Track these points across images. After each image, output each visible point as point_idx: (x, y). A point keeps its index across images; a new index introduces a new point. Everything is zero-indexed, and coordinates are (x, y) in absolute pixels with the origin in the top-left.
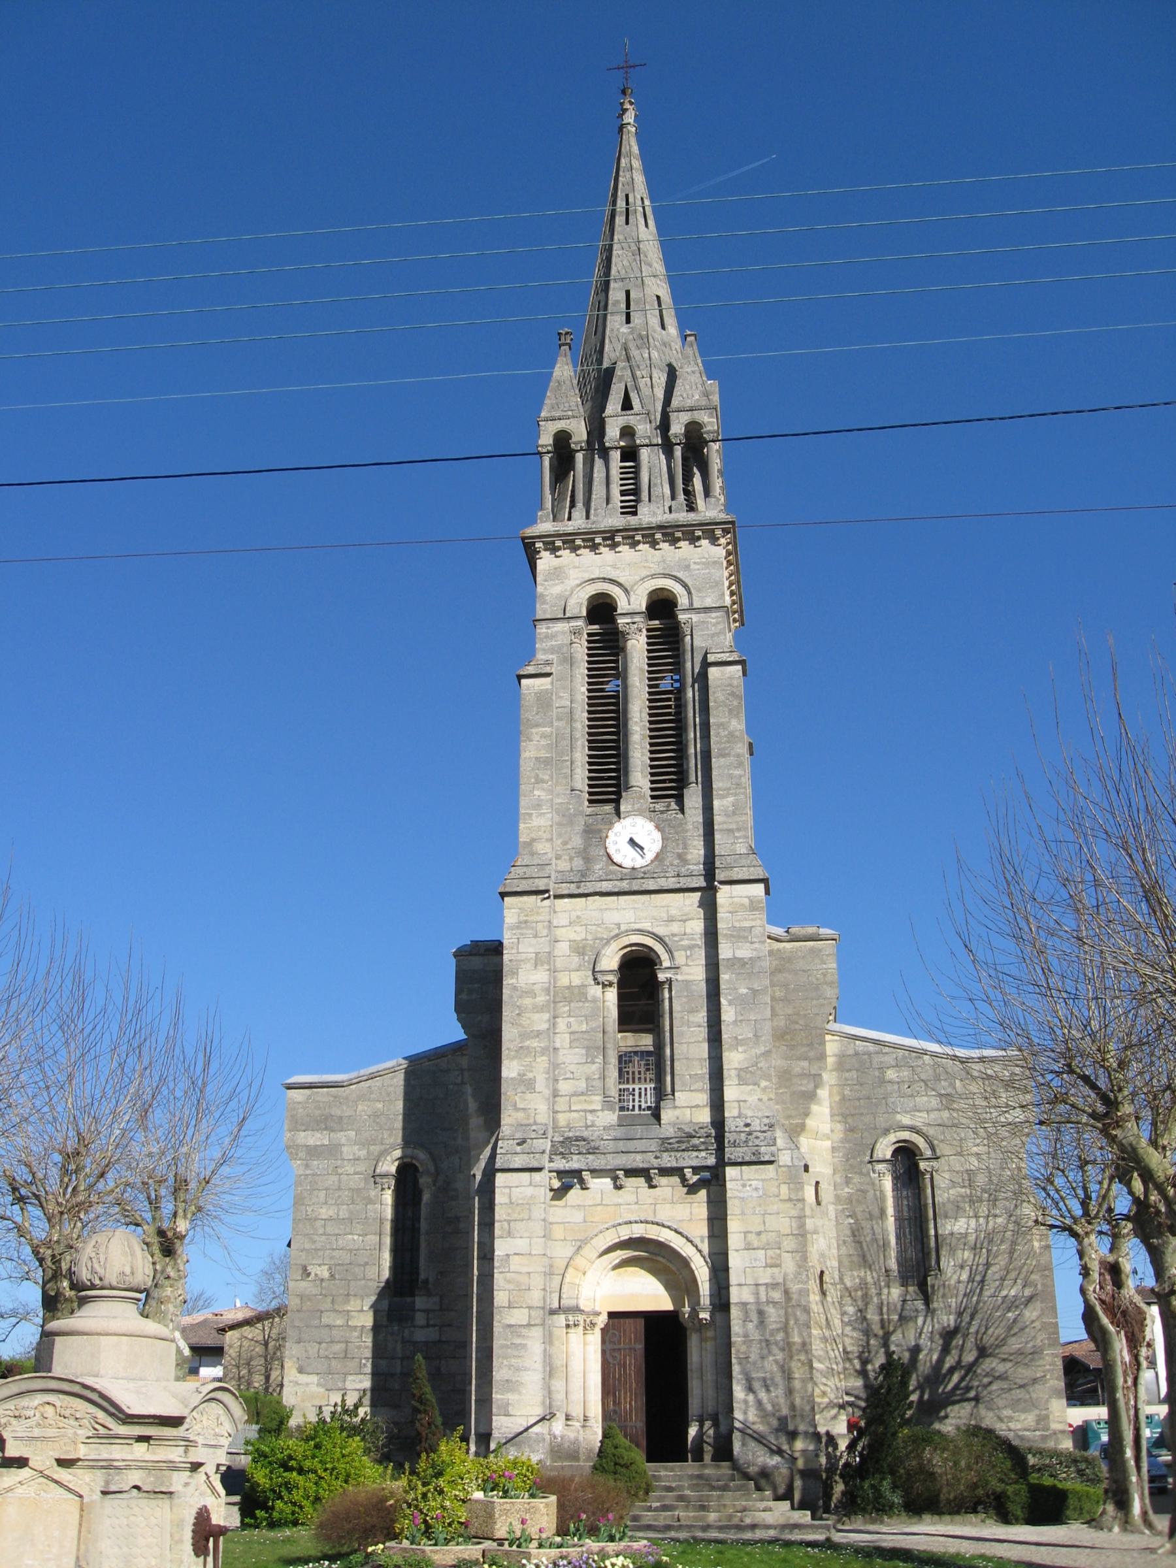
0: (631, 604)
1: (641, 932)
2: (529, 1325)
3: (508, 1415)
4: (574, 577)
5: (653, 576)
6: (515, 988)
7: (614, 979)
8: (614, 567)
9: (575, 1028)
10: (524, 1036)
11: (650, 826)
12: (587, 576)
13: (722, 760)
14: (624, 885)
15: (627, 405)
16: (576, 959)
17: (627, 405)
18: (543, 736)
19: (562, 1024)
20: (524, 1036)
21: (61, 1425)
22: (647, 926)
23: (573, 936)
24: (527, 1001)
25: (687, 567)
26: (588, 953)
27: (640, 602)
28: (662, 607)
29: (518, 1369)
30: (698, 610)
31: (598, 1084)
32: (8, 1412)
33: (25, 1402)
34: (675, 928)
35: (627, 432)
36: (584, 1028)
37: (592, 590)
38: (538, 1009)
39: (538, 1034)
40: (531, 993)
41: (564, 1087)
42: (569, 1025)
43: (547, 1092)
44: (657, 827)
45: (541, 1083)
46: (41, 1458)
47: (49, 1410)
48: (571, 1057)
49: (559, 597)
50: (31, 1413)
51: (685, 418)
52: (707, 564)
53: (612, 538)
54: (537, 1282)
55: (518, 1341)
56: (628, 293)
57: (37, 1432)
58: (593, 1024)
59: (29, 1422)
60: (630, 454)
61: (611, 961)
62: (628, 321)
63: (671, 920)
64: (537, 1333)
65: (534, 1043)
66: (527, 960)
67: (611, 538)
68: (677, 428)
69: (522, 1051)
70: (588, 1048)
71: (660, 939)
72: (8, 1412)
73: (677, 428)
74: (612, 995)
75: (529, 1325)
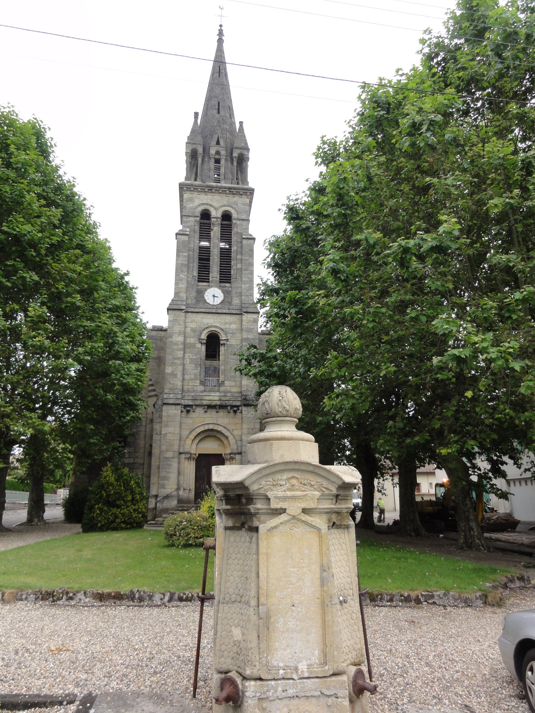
0: (216, 214)
1: (216, 327)
2: (173, 457)
3: (164, 488)
4: (197, 202)
5: (224, 206)
6: (171, 342)
7: (205, 341)
8: (211, 200)
9: (191, 357)
10: (174, 359)
11: (220, 291)
12: (201, 202)
13: (246, 272)
14: (208, 310)
15: (218, 143)
16: (192, 334)
17: (218, 143)
18: (184, 256)
19: (187, 355)
20: (174, 359)
21: (303, 489)
22: (218, 325)
23: (192, 326)
24: (176, 347)
25: (237, 204)
26: (197, 332)
27: (219, 215)
28: (227, 217)
29: (169, 473)
30: (239, 220)
31: (199, 377)
32: (268, 483)
33: (278, 476)
34: (227, 326)
35: (218, 153)
36: (194, 357)
37: (201, 209)
38: (178, 350)
39: (179, 358)
40: (177, 344)
41: (187, 377)
42: (189, 356)
43: (181, 378)
44: (223, 292)
45: (179, 376)
46: (294, 508)
47: (294, 481)
48: (190, 367)
49: (191, 208)
50: (284, 483)
51: (239, 151)
52: (244, 204)
53: (211, 190)
54: (176, 443)
55: (169, 463)
56: (219, 103)
57: (289, 494)
58: (197, 356)
59: (284, 488)
60: (217, 161)
61: (204, 336)
62: (219, 113)
63: (226, 323)
64: (176, 460)
65: (178, 361)
66: (176, 333)
67: (211, 189)
68: (235, 154)
69: (173, 364)
70: (196, 365)
71: (222, 330)
72: (268, 483)
73: (235, 154)
74: (204, 348)
75: (173, 457)
